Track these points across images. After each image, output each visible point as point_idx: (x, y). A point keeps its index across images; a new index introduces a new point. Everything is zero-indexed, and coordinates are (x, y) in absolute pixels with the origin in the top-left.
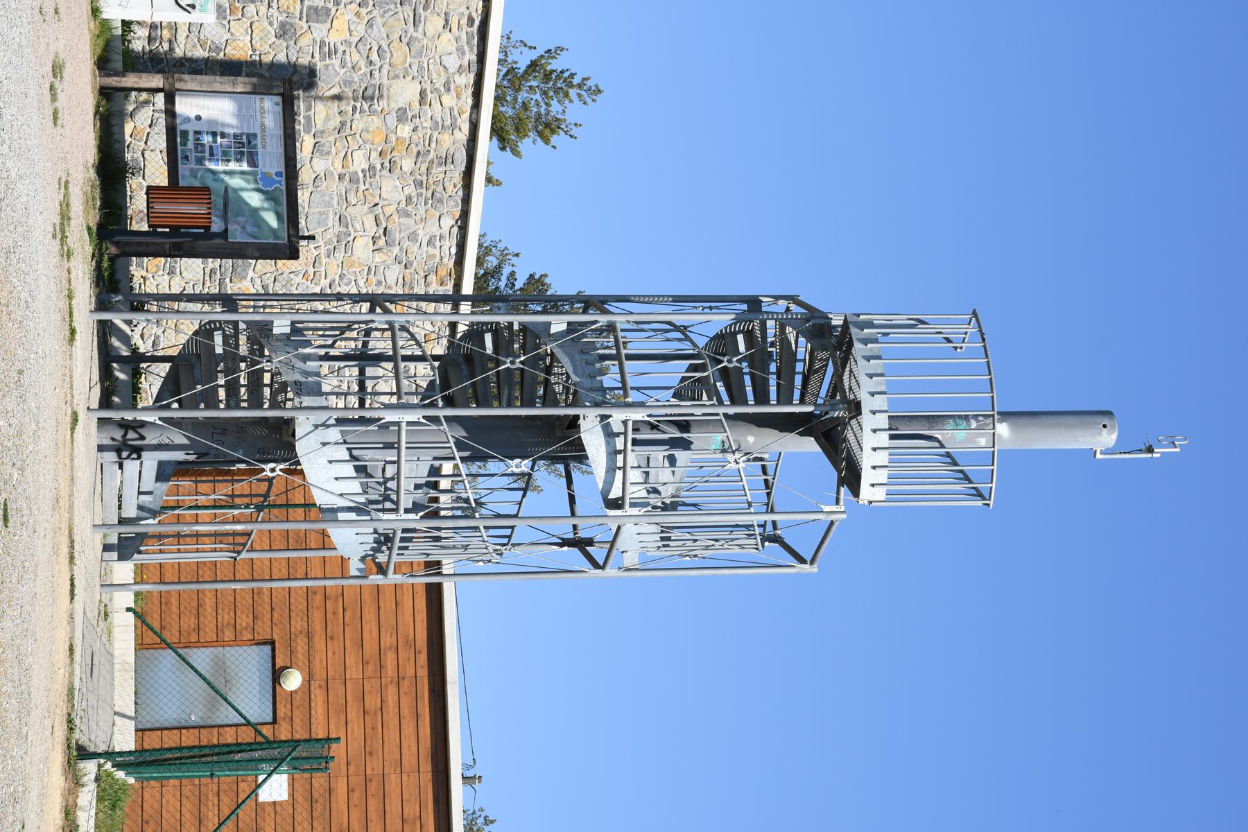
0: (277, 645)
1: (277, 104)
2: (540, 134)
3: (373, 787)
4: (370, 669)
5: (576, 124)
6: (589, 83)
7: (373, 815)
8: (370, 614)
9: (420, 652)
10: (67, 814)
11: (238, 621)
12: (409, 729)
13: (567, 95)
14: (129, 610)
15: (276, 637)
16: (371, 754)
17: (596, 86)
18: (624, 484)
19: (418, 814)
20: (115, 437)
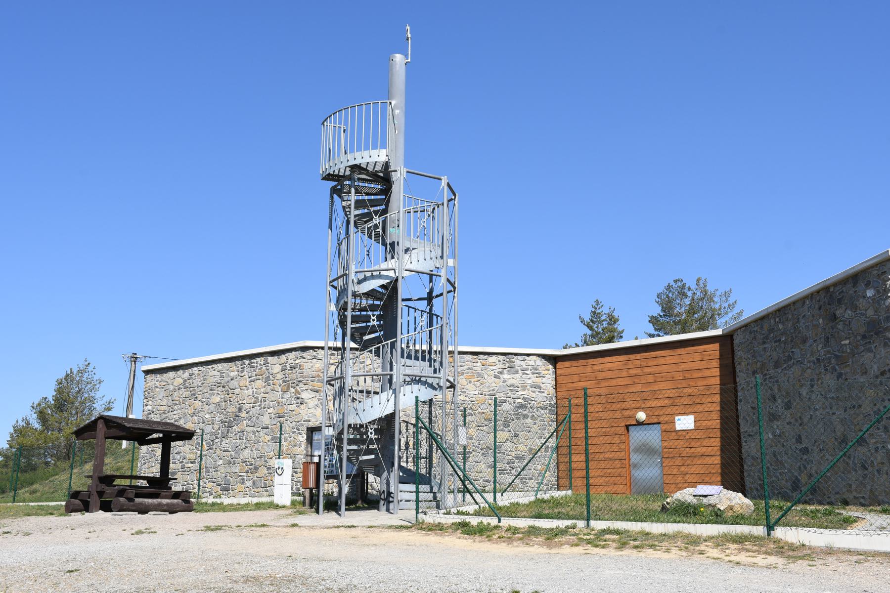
0: (628, 423)
1: (315, 434)
2: (615, 323)
3: (688, 376)
4: (637, 381)
5: (610, 309)
6: (594, 305)
7: (700, 375)
8: (614, 382)
9: (629, 358)
10: (430, 530)
11: (617, 442)
12: (662, 361)
13: (599, 313)
14: (502, 495)
15: (623, 424)
16: (673, 378)
17: (595, 302)
18: (387, 270)
19: (699, 354)
20: (383, 504)
